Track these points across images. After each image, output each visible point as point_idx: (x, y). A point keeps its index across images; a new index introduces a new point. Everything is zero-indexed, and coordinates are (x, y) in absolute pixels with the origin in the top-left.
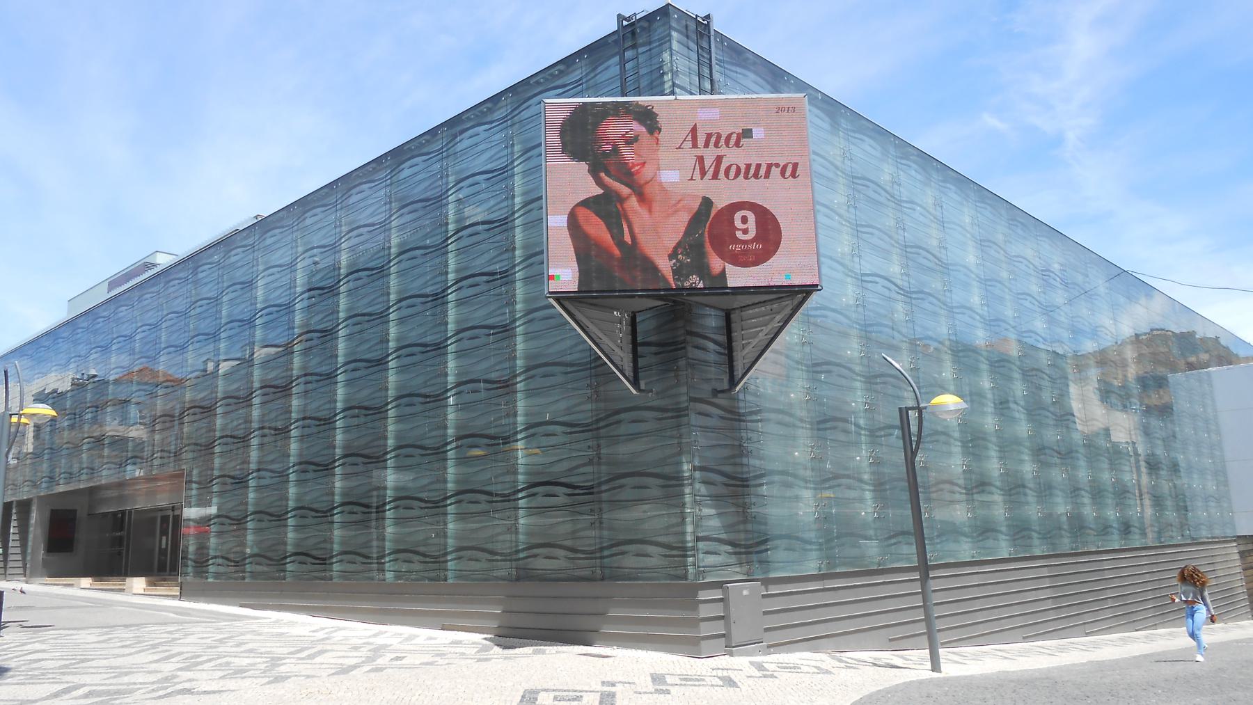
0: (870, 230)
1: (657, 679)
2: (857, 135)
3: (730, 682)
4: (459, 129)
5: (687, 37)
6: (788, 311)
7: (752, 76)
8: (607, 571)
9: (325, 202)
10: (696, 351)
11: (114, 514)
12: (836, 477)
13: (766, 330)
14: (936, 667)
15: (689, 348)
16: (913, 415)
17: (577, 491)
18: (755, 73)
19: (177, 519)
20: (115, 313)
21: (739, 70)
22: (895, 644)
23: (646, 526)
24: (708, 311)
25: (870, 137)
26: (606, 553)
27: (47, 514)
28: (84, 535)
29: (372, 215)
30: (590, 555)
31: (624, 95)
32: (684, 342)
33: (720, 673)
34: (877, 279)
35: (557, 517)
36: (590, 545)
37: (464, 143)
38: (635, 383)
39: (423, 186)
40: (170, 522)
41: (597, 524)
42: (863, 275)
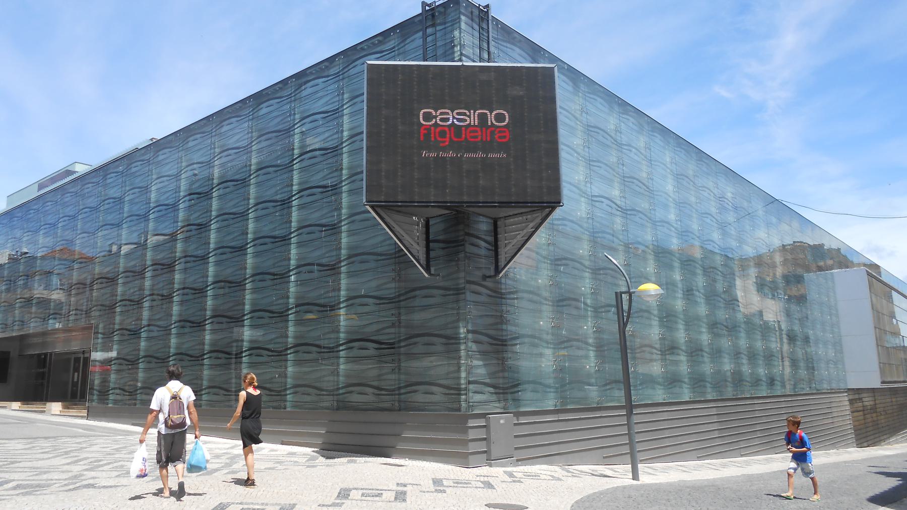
1: (437, 482)
2: (592, 96)
3: (489, 485)
4: (304, 80)
5: (472, 20)
6: (538, 220)
8: (403, 405)
10: (472, 248)
11: (39, 355)
12: (569, 340)
14: (635, 476)
15: (467, 246)
16: (625, 297)
17: (383, 346)
18: (520, 48)
19: (87, 360)
21: (508, 45)
22: (608, 460)
23: (432, 372)
24: (481, 219)
26: (403, 391)
29: (238, 141)
30: (391, 392)
32: (463, 240)
33: (482, 479)
34: (603, 200)
37: (307, 91)
38: (427, 269)
40: (82, 362)
41: (397, 370)
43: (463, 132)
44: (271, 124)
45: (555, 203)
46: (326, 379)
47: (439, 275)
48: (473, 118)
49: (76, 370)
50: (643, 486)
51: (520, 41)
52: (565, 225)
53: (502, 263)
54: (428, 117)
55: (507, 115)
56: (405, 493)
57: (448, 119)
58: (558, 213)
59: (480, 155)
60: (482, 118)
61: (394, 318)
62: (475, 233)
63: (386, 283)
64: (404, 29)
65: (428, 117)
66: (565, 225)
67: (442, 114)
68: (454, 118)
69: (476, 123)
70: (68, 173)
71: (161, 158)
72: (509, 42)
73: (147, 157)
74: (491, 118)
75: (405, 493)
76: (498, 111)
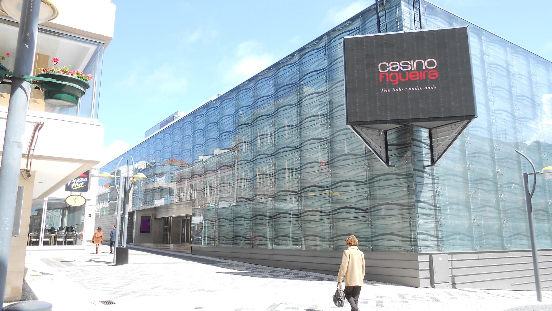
0: (499, 89)
4: (304, 52)
5: (409, 3)
6: (460, 128)
7: (439, 19)
8: (374, 247)
9: (229, 97)
11: (164, 218)
12: (484, 206)
13: (449, 137)
15: (412, 147)
17: (360, 211)
18: (441, 18)
20: (164, 136)
21: (432, 17)
22: (517, 288)
23: (391, 227)
24: (422, 129)
25: (498, 44)
26: (374, 239)
27: (140, 218)
28: (155, 227)
29: (267, 92)
31: (379, 32)
32: (410, 143)
33: (430, 296)
34: (502, 112)
35: (352, 222)
36: (365, 235)
37: (306, 58)
38: (387, 162)
39: (288, 79)
40: (185, 221)
41: (370, 226)
42: (495, 110)
43: (407, 75)
44: (286, 80)
45: (471, 116)
46: (326, 231)
47: (394, 166)
48: (413, 65)
49: (183, 226)
50: (546, 306)
51: (441, 13)
52: (477, 131)
53: (435, 158)
54: (384, 67)
55: (380, 64)
56: (382, 302)
57: (397, 68)
58: (474, 122)
59: (419, 88)
60: (419, 65)
61: (366, 194)
62: (417, 138)
63: (360, 173)
64: (363, 15)
65: (384, 67)
66: (477, 131)
67: (392, 64)
68: (400, 66)
69: (415, 69)
70: (172, 118)
71: (224, 105)
72: (431, 15)
73: (216, 105)
74: (425, 65)
75: (382, 302)
76: (429, 60)
